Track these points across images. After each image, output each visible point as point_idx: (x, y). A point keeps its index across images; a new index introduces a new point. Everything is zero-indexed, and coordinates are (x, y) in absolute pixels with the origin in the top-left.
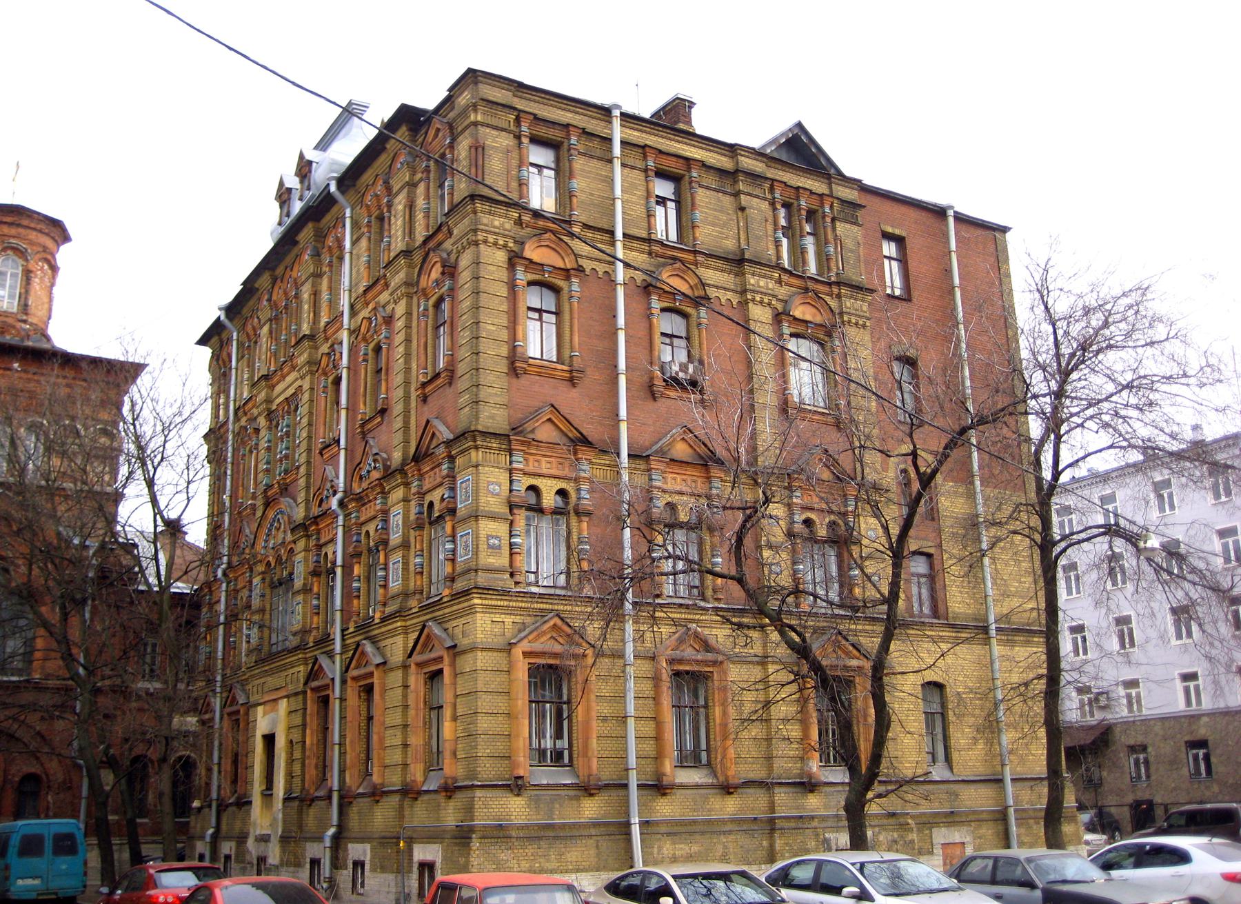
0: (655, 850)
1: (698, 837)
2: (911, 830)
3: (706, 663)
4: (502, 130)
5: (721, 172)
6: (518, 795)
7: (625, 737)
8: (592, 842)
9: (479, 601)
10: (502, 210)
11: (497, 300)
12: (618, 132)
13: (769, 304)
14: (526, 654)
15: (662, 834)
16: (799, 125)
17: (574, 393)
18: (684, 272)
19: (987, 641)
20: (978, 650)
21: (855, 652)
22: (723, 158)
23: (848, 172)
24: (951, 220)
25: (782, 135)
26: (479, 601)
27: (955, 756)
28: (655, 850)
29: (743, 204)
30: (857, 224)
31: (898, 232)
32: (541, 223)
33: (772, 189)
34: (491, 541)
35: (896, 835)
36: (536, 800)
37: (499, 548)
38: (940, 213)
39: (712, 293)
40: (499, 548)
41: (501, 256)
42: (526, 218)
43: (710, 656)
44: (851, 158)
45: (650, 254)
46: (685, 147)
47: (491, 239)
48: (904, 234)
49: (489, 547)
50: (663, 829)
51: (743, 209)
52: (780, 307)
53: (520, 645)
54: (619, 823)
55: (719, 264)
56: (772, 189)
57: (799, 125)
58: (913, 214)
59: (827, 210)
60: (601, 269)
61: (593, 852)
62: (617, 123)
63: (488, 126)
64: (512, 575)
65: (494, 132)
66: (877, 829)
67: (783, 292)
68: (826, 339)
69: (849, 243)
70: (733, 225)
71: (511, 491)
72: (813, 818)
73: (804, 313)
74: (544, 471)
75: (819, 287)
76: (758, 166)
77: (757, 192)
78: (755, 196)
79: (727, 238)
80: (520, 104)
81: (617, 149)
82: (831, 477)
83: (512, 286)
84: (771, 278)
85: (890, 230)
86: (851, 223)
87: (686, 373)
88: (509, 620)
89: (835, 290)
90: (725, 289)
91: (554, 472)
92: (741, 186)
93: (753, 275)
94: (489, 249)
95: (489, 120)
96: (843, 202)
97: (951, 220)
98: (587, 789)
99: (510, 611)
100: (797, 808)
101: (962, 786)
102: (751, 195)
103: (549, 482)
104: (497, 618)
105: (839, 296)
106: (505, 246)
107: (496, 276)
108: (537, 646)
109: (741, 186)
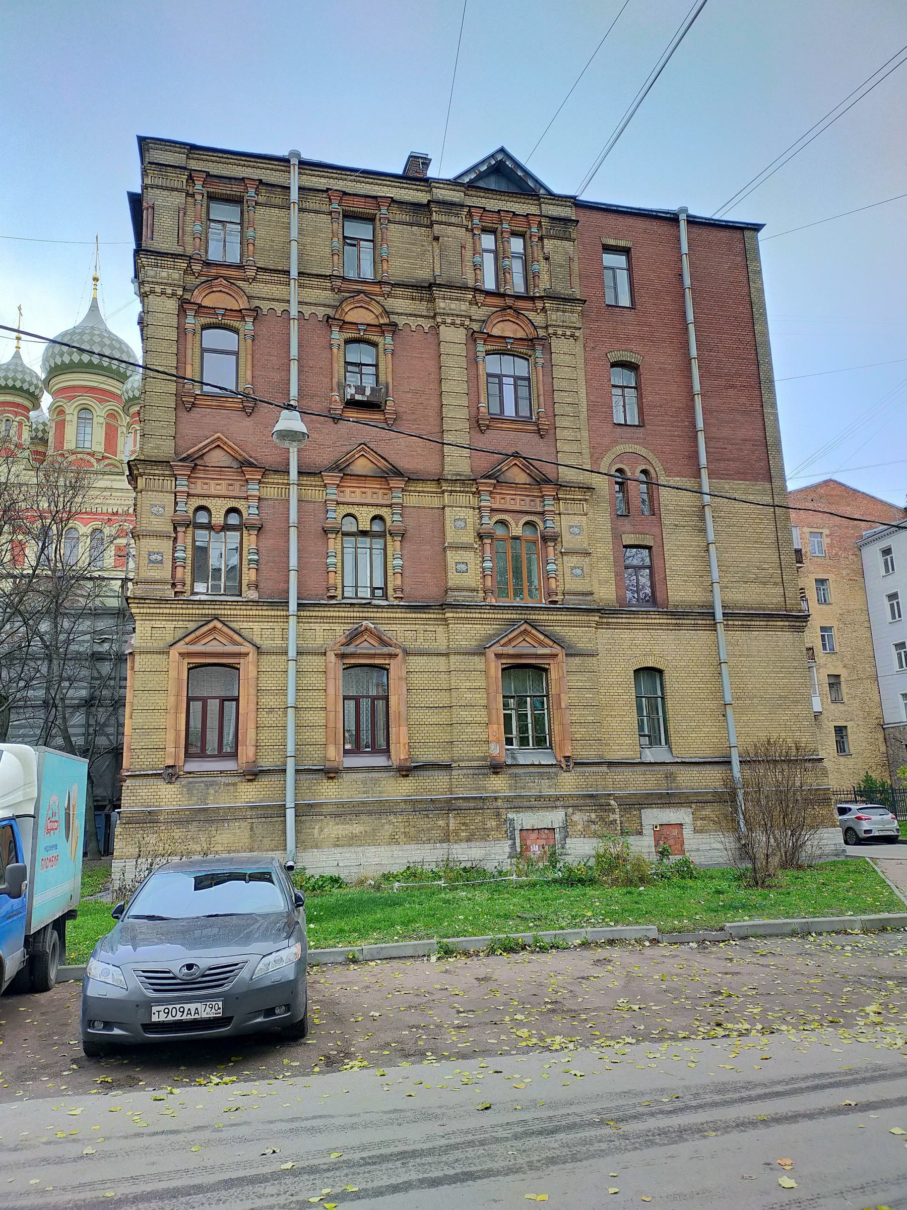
0: (316, 831)
1: (363, 817)
2: (614, 812)
3: (383, 656)
4: (176, 190)
5: (416, 206)
6: (170, 783)
7: (285, 727)
8: (244, 824)
9: (138, 611)
10: (169, 262)
11: (165, 344)
12: (294, 180)
13: (462, 325)
14: (498, 656)
15: (325, 816)
16: (502, 150)
17: (248, 422)
18: (369, 304)
19: (713, 627)
20: (704, 636)
21: (547, 640)
22: (419, 194)
23: (556, 190)
24: (683, 225)
25: (482, 162)
26: (138, 611)
27: (673, 739)
28: (316, 831)
29: (436, 233)
30: (568, 239)
31: (622, 243)
32: (214, 271)
33: (470, 215)
34: (153, 557)
35: (593, 816)
36: (190, 788)
37: (161, 562)
38: (672, 219)
39: (401, 321)
40: (161, 562)
41: (172, 305)
42: (197, 267)
43: (385, 650)
44: (559, 172)
45: (333, 290)
46: (376, 188)
47: (158, 289)
48: (629, 244)
49: (150, 561)
50: (331, 809)
51: (436, 239)
52: (476, 327)
53: (492, 649)
54: (280, 806)
55: (408, 292)
56: (470, 215)
57: (502, 150)
58: (641, 224)
59: (534, 230)
60: (279, 307)
61: (247, 833)
62: (295, 171)
63: (157, 187)
64: (174, 585)
65: (166, 193)
66: (570, 810)
67: (478, 313)
68: (530, 352)
69: (557, 258)
70: (429, 255)
71: (175, 511)
72: (496, 798)
73: (503, 331)
74: (213, 492)
75: (520, 304)
76: (455, 196)
77: (453, 220)
78: (450, 224)
79: (421, 267)
80: (193, 165)
81: (294, 195)
82: (528, 480)
83: (181, 331)
84: (464, 301)
85: (612, 242)
86: (562, 239)
87: (363, 394)
88: (170, 625)
89: (539, 305)
90: (415, 315)
91: (224, 492)
92: (435, 217)
93: (444, 298)
94: (158, 299)
95: (159, 182)
96: (553, 219)
97: (683, 225)
98: (253, 774)
99: (172, 617)
100: (478, 789)
101: (682, 768)
102: (445, 224)
103: (219, 501)
104: (158, 624)
105: (544, 310)
106: (173, 295)
107: (165, 323)
108: (509, 650)
109: (435, 217)
